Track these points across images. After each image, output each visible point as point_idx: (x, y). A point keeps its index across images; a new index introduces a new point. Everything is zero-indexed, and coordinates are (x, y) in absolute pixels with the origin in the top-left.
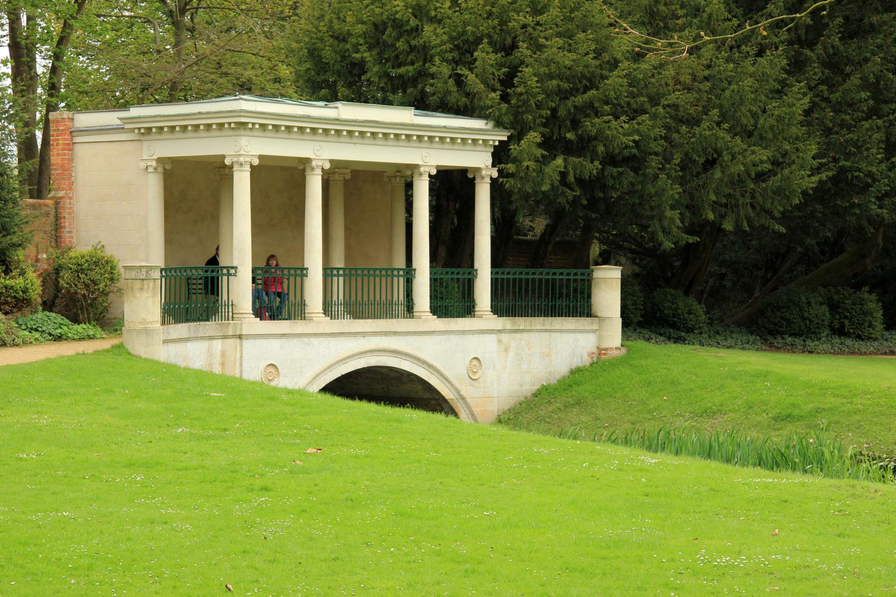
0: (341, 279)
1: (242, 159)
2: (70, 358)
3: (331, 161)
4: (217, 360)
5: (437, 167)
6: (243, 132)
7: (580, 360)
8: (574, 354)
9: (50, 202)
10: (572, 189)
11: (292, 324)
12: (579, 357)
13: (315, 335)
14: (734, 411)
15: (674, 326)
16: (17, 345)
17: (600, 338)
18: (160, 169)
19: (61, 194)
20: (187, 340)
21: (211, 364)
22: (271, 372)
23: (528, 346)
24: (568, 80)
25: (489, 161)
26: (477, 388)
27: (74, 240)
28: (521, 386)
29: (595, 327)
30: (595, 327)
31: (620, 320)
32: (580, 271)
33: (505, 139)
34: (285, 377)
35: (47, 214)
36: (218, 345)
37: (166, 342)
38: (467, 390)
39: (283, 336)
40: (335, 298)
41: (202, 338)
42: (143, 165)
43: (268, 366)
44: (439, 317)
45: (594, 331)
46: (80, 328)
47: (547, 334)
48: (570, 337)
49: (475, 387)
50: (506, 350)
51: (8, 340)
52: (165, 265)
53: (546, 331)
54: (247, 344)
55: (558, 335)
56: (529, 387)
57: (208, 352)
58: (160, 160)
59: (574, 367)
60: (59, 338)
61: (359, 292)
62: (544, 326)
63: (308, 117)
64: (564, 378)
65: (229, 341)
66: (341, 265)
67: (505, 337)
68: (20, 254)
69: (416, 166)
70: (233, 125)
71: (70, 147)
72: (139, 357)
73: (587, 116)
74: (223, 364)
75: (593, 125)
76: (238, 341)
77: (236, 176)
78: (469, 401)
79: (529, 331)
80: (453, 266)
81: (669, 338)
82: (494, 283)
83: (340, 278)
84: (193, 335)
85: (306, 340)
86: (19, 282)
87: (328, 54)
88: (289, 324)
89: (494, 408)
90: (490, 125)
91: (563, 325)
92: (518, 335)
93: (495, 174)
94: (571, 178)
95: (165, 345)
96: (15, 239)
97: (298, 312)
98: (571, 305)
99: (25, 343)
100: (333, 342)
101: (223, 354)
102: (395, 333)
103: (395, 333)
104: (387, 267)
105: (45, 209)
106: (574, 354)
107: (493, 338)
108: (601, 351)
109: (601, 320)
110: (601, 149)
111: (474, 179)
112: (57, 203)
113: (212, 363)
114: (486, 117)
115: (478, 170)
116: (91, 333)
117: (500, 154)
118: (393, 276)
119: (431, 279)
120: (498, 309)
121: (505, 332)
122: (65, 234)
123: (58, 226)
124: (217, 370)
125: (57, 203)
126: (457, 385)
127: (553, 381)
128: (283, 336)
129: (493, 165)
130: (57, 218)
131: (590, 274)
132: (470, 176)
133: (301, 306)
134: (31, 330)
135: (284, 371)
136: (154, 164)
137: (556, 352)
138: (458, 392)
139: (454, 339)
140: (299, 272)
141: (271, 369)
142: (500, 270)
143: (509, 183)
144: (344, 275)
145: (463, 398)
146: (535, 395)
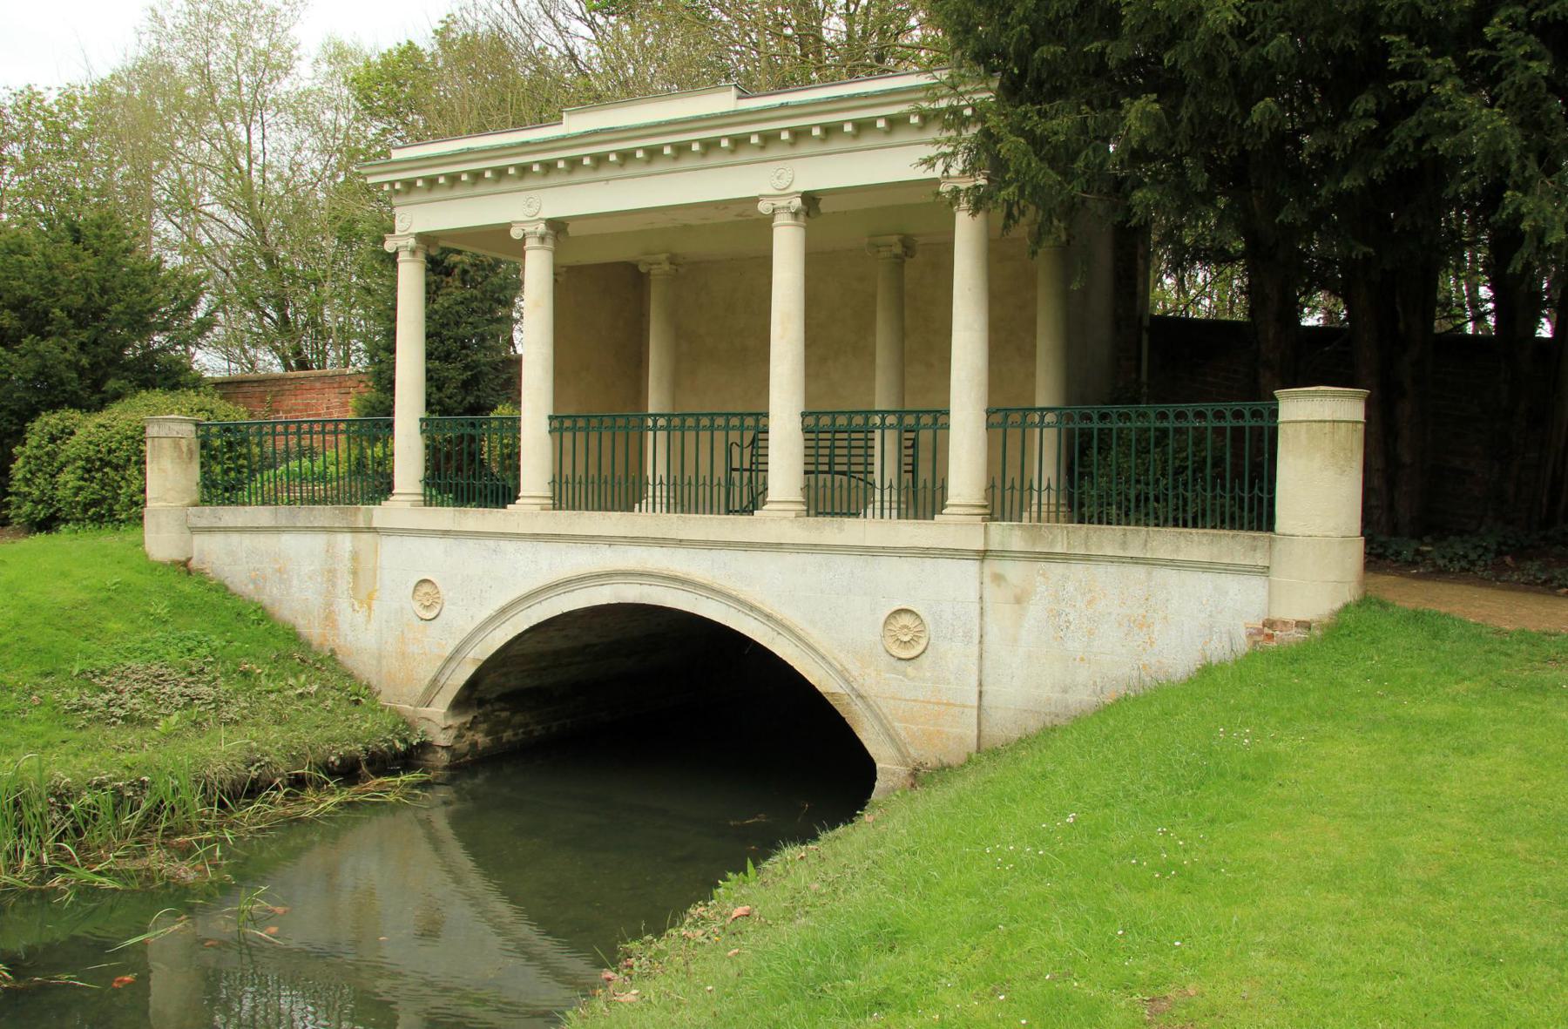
7: (1227, 647)
8: (1211, 627)
11: (457, 514)
12: (1225, 638)
20: (277, 530)
22: (427, 593)
23: (1088, 597)
26: (912, 679)
28: (1065, 691)
32: (1246, 407)
34: (453, 604)
36: (345, 542)
39: (446, 533)
43: (416, 586)
45: (1265, 571)
47: (1139, 572)
49: (905, 675)
52: (554, 411)
53: (1135, 561)
54: (388, 545)
57: (328, 551)
61: (606, 461)
62: (1124, 549)
67: (1014, 571)
70: (398, 186)
79: (1087, 558)
83: (565, 434)
85: (491, 543)
88: (452, 514)
91: (1178, 549)
92: (1057, 569)
97: (503, 493)
98: (1246, 496)
100: (546, 551)
101: (355, 556)
102: (680, 543)
103: (680, 543)
104: (883, 409)
106: (1211, 627)
113: (335, 570)
121: (1014, 559)
128: (446, 533)
131: (1274, 414)
133: (600, 487)
135: (451, 594)
137: (1165, 618)
140: (926, 419)
141: (426, 588)
145: (860, 696)
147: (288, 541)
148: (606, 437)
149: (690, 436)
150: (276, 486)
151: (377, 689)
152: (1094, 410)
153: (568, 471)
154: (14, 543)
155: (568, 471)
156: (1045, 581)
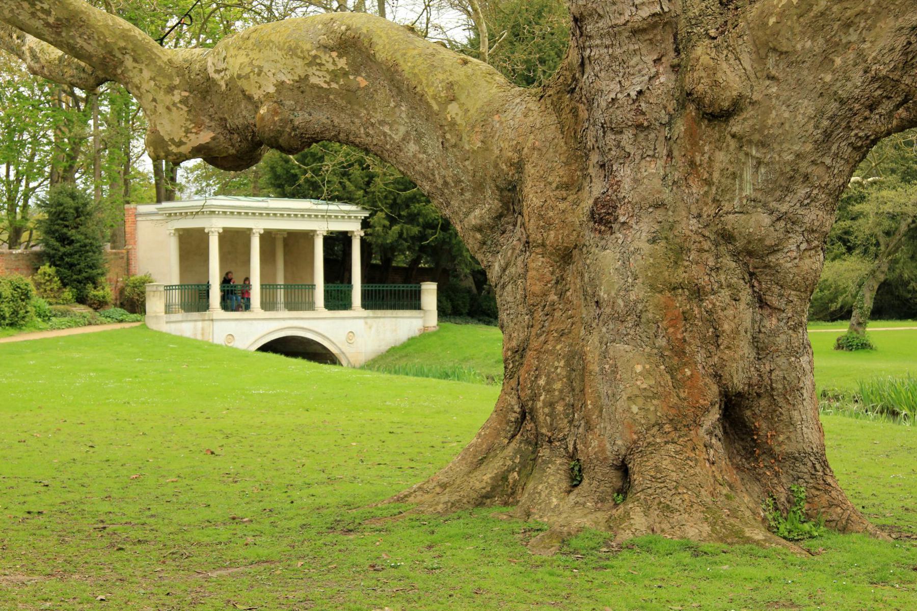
0: (282, 291)
1: (213, 230)
2: (118, 330)
3: (224, 228)
4: (199, 332)
5: (264, 229)
6: (213, 216)
9: (124, 251)
10: (407, 242)
13: (255, 319)
14: (478, 358)
15: (488, 315)
16: (98, 324)
17: (424, 321)
18: (177, 234)
19: (130, 247)
20: (182, 321)
21: (196, 334)
24: (402, 184)
25: (359, 227)
27: (137, 271)
29: (422, 315)
30: (422, 315)
31: (436, 312)
33: (368, 215)
35: (122, 258)
36: (200, 324)
37: (167, 322)
38: (346, 349)
40: (279, 300)
41: (190, 321)
42: (168, 232)
44: (266, 310)
46: (133, 316)
47: (394, 319)
48: (408, 321)
50: (370, 328)
51: (93, 322)
52: (181, 282)
54: (216, 324)
55: (401, 320)
56: (384, 347)
58: (177, 230)
59: (410, 337)
60: (121, 321)
63: (250, 207)
64: (404, 343)
65: (206, 322)
66: (282, 283)
67: (369, 321)
68: (103, 279)
69: (315, 231)
71: (135, 223)
72: (152, 330)
73: (414, 203)
74: (203, 334)
75: (415, 207)
76: (211, 322)
77: (211, 238)
78: (348, 355)
79: (384, 317)
80: (372, 283)
81: (479, 320)
82: (327, 292)
84: (185, 319)
85: (250, 322)
86: (101, 293)
87: (279, 170)
89: (362, 359)
90: (359, 208)
92: (377, 320)
93: (363, 234)
94: (405, 235)
95: (168, 325)
96: (100, 271)
99: (102, 323)
101: (203, 329)
102: (302, 319)
103: (302, 319)
105: (121, 255)
107: (362, 321)
108: (425, 328)
109: (425, 311)
110: (421, 220)
111: (351, 237)
112: (128, 252)
114: (357, 204)
115: (353, 232)
116: (139, 318)
117: (365, 224)
118: (277, 288)
119: (325, 291)
120: (366, 305)
122: (132, 268)
123: (128, 264)
124: (199, 337)
125: (128, 252)
126: (340, 346)
127: (398, 344)
129: (362, 228)
130: (128, 259)
131: (420, 287)
132: (349, 235)
134: (107, 317)
136: (173, 231)
138: (340, 350)
139: (338, 322)
141: (231, 337)
142: (330, 285)
143: (369, 239)
144: (284, 288)
145: (343, 353)
146: (388, 352)
147: (184, 325)
148: (300, 292)
149: (268, 290)
150: (60, 304)
151: (884, 415)
152: (367, 285)
153: (264, 300)
154: (380, 346)
155: (264, 300)
156: (375, 323)
